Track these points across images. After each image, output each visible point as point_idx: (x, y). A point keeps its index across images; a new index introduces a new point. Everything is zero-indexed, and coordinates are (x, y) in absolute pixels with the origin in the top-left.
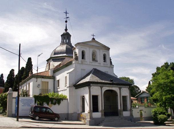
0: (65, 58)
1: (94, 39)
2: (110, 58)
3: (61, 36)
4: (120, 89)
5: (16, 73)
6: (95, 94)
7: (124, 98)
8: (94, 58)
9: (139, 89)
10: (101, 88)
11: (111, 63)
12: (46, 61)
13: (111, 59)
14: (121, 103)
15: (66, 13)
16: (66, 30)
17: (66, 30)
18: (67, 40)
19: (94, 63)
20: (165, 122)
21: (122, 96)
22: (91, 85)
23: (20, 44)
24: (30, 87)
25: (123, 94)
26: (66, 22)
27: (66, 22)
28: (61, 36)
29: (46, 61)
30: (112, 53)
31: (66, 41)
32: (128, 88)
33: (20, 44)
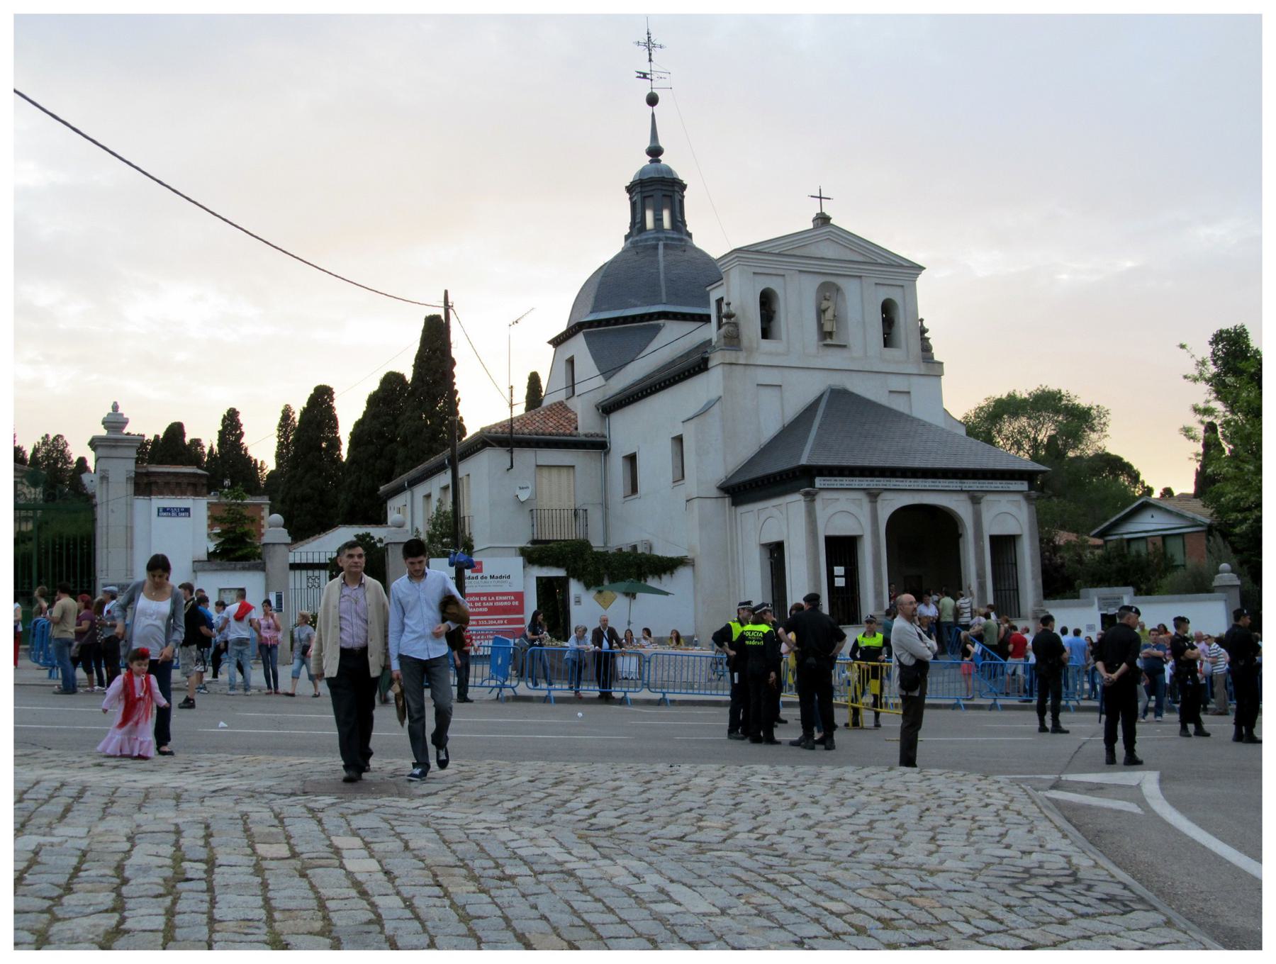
0: (658, 329)
1: (823, 220)
2: (922, 320)
3: (630, 189)
4: (975, 499)
5: (349, 413)
6: (843, 527)
7: (1003, 546)
8: (827, 328)
9: (1135, 477)
10: (873, 495)
11: (926, 348)
12: (550, 342)
13: (923, 331)
14: (981, 576)
16: (655, 152)
17: (655, 152)
18: (666, 215)
19: (834, 359)
20: (336, 443)
21: (993, 538)
22: (819, 482)
23: (446, 292)
24: (416, 505)
25: (994, 527)
27: (652, 100)
28: (630, 189)
29: (550, 342)
30: (932, 303)
31: (658, 220)
32: (1019, 497)
33: (446, 292)
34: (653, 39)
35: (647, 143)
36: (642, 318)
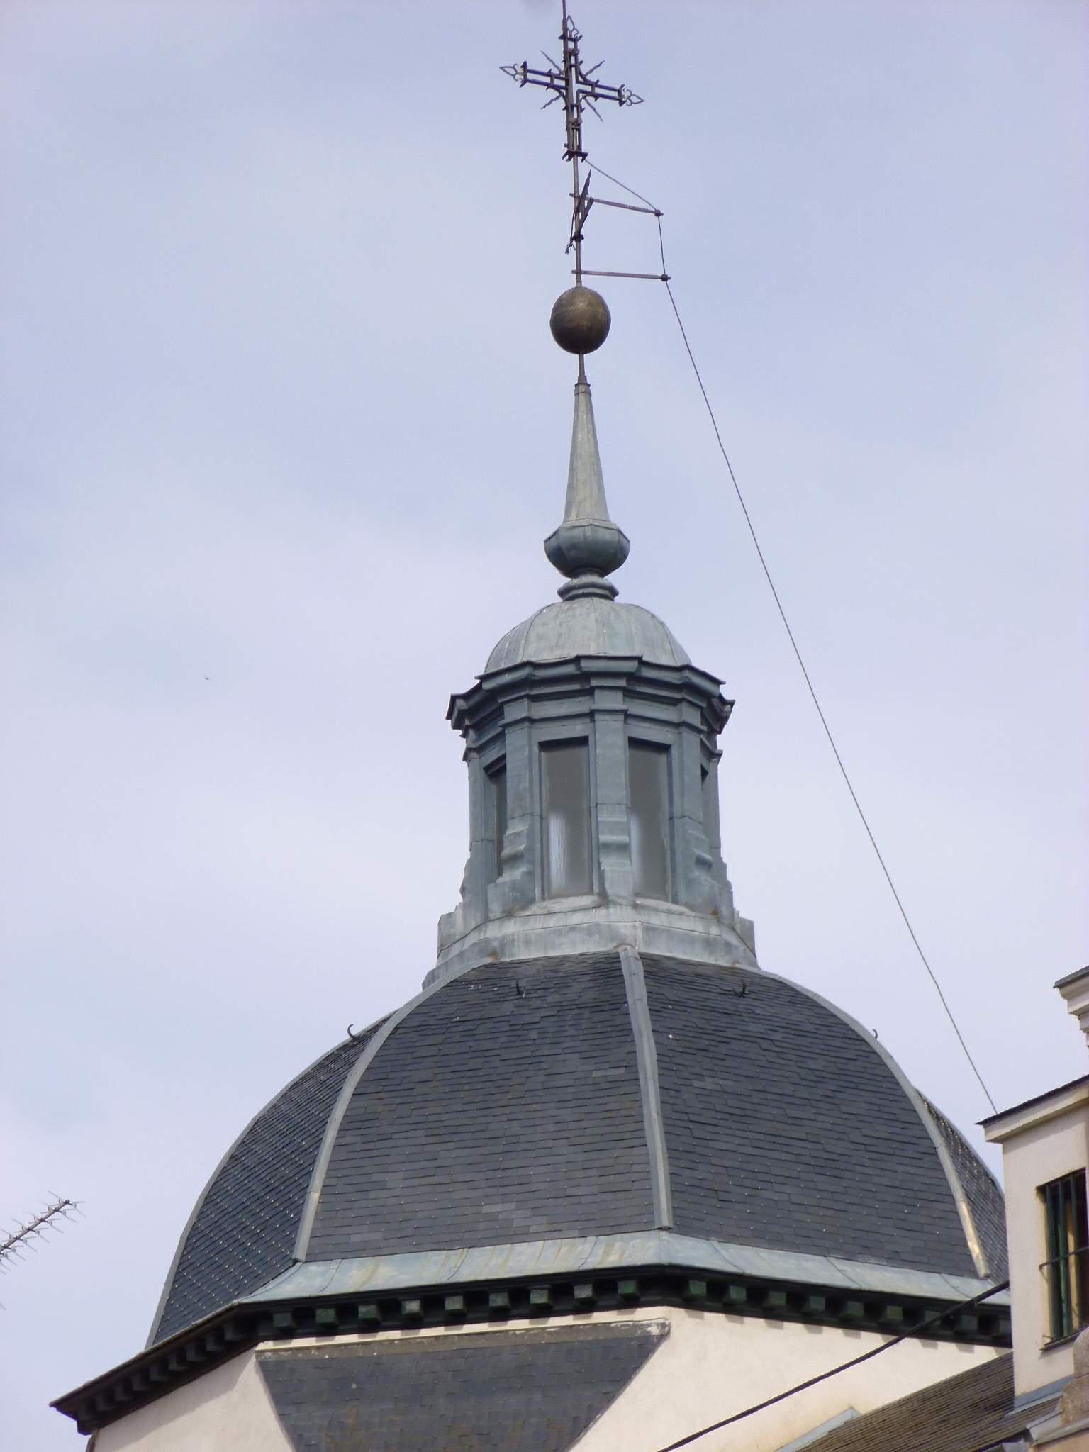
3: (478, 712)
15: (571, 83)
26: (580, 329)
27: (580, 329)
28: (478, 712)
34: (587, 59)
35: (550, 518)
36: (562, 1291)
